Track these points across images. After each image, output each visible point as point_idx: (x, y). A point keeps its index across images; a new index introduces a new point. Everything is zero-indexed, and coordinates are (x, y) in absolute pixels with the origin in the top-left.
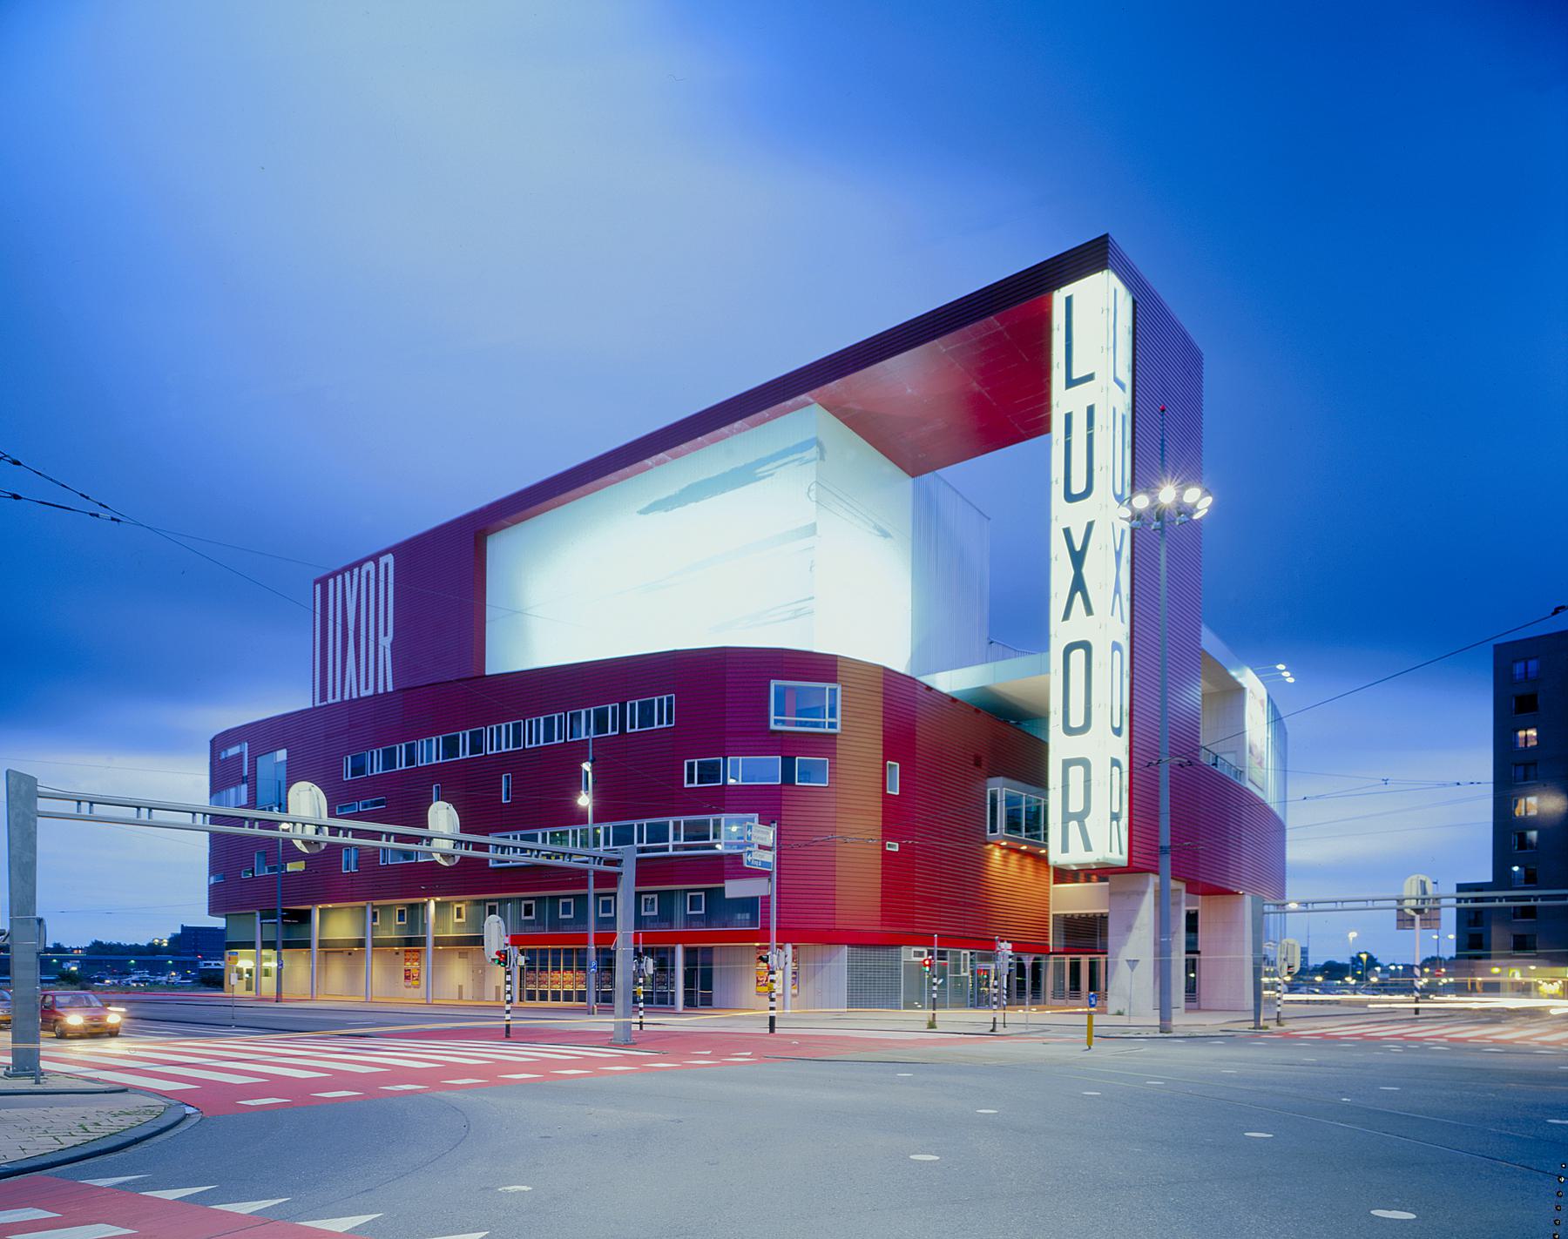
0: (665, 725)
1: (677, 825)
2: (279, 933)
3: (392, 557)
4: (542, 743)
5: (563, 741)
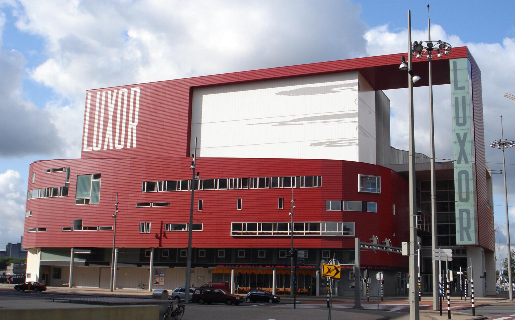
1: (260, 225)
2: (407, 300)
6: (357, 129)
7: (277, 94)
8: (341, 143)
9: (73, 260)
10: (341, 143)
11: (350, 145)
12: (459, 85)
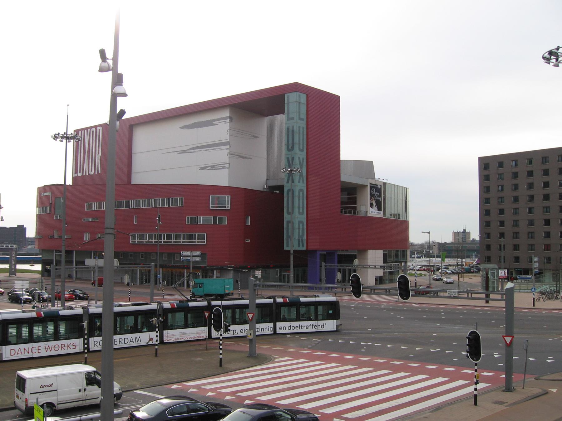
0: (181, 206)
3: (101, 128)
4: (146, 207)
5: (152, 207)
6: (228, 155)
7: (182, 128)
8: (218, 167)
9: (74, 268)
10: (218, 167)
11: (224, 168)
12: (291, 116)
